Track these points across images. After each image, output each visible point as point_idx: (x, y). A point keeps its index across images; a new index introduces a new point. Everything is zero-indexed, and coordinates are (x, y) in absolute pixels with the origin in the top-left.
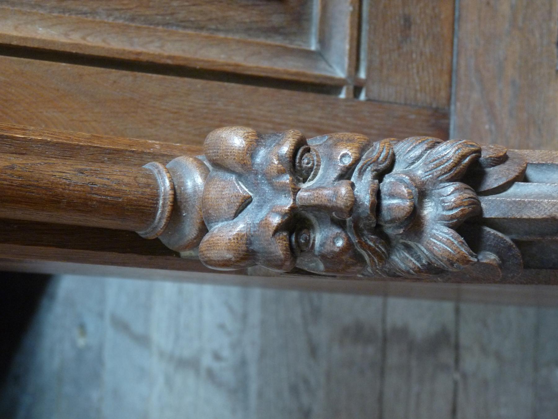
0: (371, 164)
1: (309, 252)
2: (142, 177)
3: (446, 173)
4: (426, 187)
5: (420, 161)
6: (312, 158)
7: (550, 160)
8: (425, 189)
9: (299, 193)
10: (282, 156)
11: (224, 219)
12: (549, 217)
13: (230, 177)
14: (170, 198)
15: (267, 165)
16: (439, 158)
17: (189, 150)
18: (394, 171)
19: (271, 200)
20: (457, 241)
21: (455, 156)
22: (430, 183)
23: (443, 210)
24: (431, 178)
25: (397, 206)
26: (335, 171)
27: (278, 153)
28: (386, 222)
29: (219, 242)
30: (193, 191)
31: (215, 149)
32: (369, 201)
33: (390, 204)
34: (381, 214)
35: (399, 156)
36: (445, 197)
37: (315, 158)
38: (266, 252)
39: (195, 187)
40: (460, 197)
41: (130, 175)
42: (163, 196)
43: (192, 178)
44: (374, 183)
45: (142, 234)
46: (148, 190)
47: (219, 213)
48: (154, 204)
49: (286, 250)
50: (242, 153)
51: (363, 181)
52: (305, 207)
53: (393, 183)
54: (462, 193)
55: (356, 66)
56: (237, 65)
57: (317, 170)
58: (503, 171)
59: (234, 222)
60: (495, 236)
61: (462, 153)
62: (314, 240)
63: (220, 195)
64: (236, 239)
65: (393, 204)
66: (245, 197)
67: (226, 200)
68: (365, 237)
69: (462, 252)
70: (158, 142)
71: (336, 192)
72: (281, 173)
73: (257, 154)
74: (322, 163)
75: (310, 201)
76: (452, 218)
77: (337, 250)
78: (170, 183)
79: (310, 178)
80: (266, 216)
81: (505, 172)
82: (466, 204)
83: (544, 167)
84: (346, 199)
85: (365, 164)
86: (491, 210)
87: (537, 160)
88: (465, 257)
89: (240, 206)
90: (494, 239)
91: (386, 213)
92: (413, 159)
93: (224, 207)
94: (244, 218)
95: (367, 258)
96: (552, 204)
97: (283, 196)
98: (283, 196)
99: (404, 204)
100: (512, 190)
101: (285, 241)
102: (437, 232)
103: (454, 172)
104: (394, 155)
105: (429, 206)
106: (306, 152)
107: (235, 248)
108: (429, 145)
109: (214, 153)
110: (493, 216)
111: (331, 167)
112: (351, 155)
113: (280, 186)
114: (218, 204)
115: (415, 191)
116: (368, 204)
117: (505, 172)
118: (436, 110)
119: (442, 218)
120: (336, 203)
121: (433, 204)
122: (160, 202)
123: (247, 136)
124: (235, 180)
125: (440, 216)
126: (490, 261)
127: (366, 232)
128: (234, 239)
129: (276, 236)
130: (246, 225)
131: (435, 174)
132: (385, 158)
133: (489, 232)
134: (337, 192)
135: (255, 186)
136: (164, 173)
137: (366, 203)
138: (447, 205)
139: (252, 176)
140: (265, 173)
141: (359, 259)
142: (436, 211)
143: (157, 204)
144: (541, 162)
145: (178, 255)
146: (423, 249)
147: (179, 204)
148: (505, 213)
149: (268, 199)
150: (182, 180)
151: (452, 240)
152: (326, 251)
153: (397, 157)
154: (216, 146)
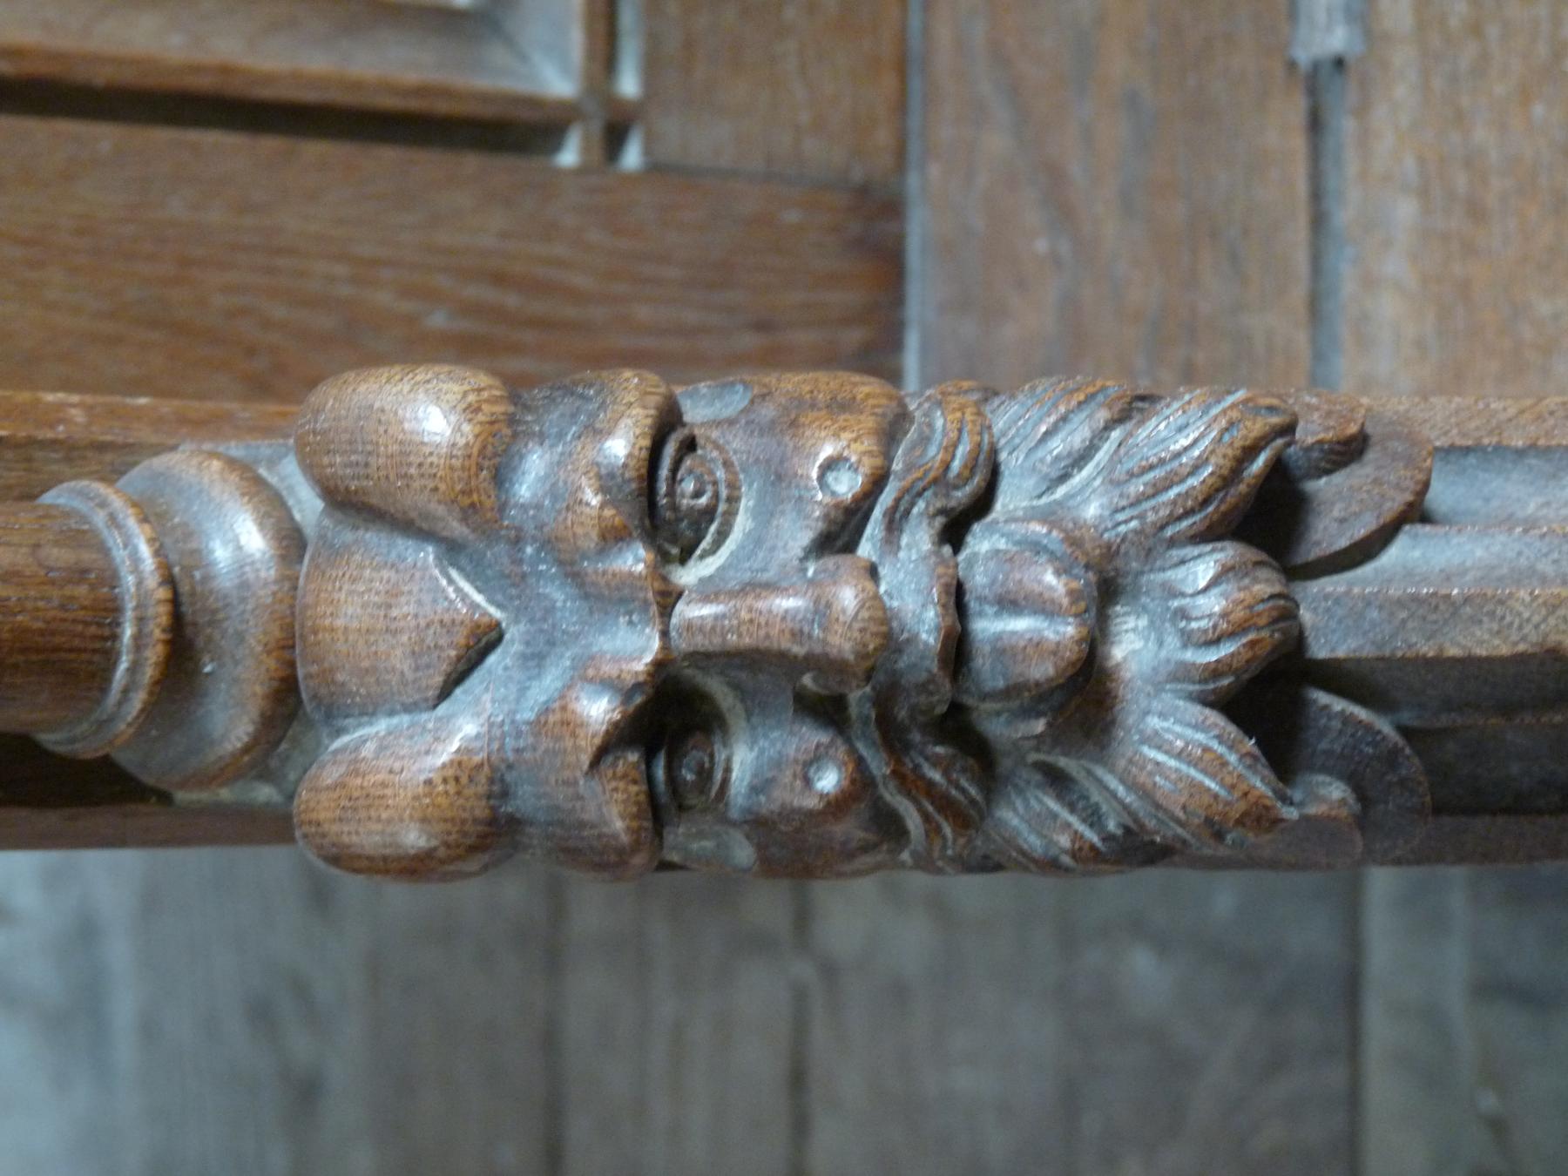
0: (924, 489)
1: (704, 811)
2: (57, 543)
3: (1188, 513)
4: (1119, 563)
5: (1089, 469)
6: (711, 473)
7: (1491, 433)
8: (1116, 570)
9: (680, 607)
10: (611, 476)
11: (398, 707)
12: (1538, 650)
13: (417, 551)
14: (160, 616)
15: (558, 506)
16: (1162, 462)
17: (183, 420)
18: (998, 506)
19: (576, 636)
20: (1237, 751)
21: (1221, 450)
22: (1132, 552)
23: (1185, 646)
24: (1135, 532)
25: (1031, 640)
26: (806, 523)
27: (598, 465)
28: (985, 697)
29: (389, 792)
30: (236, 581)
31: (355, 452)
32: (938, 628)
33: (1003, 632)
34: (970, 670)
35: (1010, 453)
36: (1188, 600)
37: (720, 474)
38: (561, 823)
39: (242, 567)
40: (1242, 595)
41: (15, 539)
42: (136, 608)
43: (230, 535)
44: (942, 561)
45: (56, 743)
46: (82, 590)
47: (378, 682)
48: (105, 639)
49: (637, 816)
50: (463, 468)
51: (902, 554)
52: (702, 659)
53: (1008, 557)
54: (1247, 581)
55: (605, 55)
56: (225, 70)
57: (731, 514)
58: (1361, 488)
59: (439, 719)
60: (1346, 719)
61: (1245, 438)
62: (728, 770)
63: (382, 619)
64: (452, 783)
65: (1014, 633)
66: (478, 626)
67: (405, 638)
68: (913, 753)
69: (1257, 793)
70: (75, 398)
71: (823, 602)
72: (613, 537)
73: (514, 470)
74: (743, 489)
75: (723, 636)
76: (1215, 671)
77: (811, 803)
78: (156, 560)
79: (704, 545)
80: (562, 697)
81: (1368, 492)
82: (1263, 621)
83: (1472, 459)
84: (862, 630)
85: (905, 491)
86: (1334, 631)
87: (1446, 433)
88: (1267, 808)
89: (459, 659)
90: (1341, 732)
91: (987, 667)
92: (1062, 465)
93: (400, 661)
94: (477, 701)
95: (913, 821)
96: (1545, 603)
97: (622, 620)
98: (622, 620)
99: (1057, 633)
100: (1395, 554)
101: (635, 782)
102: (1165, 725)
103: (1218, 507)
104: (994, 452)
105: (1127, 631)
106: (895, 540)
107: (449, 814)
108: (1116, 409)
109: (350, 465)
110: (1341, 653)
111: (789, 507)
112: (859, 461)
113: (613, 584)
114: (376, 653)
115: (1085, 580)
116: (931, 641)
117: (1368, 492)
118: (863, 191)
119: (1181, 673)
120: (824, 642)
121: (1143, 622)
122: (123, 632)
123: (476, 405)
124: (436, 566)
125: (1171, 667)
126: (1331, 809)
127: (916, 737)
128: (445, 781)
129: (602, 767)
130: (485, 729)
131: (1151, 517)
132: (970, 466)
133: (1326, 707)
134: (829, 605)
135: (514, 585)
136: (132, 523)
137: (924, 636)
138: (1199, 629)
139: (501, 548)
140: (553, 540)
141: (889, 827)
142: (1156, 648)
143: (115, 637)
144: (1459, 442)
145: (165, 798)
146: (1113, 783)
147: (189, 631)
148: (1384, 638)
149: (564, 632)
150: (193, 545)
151: (1221, 749)
152: (775, 807)
153: (1003, 456)
154: (359, 440)
